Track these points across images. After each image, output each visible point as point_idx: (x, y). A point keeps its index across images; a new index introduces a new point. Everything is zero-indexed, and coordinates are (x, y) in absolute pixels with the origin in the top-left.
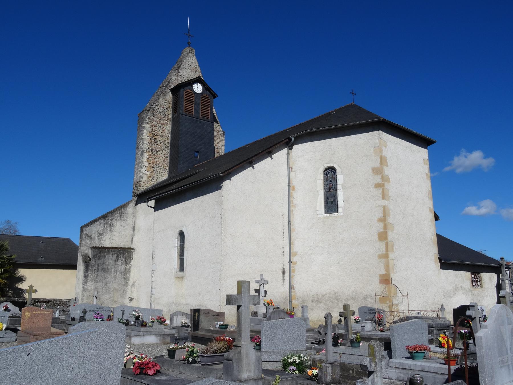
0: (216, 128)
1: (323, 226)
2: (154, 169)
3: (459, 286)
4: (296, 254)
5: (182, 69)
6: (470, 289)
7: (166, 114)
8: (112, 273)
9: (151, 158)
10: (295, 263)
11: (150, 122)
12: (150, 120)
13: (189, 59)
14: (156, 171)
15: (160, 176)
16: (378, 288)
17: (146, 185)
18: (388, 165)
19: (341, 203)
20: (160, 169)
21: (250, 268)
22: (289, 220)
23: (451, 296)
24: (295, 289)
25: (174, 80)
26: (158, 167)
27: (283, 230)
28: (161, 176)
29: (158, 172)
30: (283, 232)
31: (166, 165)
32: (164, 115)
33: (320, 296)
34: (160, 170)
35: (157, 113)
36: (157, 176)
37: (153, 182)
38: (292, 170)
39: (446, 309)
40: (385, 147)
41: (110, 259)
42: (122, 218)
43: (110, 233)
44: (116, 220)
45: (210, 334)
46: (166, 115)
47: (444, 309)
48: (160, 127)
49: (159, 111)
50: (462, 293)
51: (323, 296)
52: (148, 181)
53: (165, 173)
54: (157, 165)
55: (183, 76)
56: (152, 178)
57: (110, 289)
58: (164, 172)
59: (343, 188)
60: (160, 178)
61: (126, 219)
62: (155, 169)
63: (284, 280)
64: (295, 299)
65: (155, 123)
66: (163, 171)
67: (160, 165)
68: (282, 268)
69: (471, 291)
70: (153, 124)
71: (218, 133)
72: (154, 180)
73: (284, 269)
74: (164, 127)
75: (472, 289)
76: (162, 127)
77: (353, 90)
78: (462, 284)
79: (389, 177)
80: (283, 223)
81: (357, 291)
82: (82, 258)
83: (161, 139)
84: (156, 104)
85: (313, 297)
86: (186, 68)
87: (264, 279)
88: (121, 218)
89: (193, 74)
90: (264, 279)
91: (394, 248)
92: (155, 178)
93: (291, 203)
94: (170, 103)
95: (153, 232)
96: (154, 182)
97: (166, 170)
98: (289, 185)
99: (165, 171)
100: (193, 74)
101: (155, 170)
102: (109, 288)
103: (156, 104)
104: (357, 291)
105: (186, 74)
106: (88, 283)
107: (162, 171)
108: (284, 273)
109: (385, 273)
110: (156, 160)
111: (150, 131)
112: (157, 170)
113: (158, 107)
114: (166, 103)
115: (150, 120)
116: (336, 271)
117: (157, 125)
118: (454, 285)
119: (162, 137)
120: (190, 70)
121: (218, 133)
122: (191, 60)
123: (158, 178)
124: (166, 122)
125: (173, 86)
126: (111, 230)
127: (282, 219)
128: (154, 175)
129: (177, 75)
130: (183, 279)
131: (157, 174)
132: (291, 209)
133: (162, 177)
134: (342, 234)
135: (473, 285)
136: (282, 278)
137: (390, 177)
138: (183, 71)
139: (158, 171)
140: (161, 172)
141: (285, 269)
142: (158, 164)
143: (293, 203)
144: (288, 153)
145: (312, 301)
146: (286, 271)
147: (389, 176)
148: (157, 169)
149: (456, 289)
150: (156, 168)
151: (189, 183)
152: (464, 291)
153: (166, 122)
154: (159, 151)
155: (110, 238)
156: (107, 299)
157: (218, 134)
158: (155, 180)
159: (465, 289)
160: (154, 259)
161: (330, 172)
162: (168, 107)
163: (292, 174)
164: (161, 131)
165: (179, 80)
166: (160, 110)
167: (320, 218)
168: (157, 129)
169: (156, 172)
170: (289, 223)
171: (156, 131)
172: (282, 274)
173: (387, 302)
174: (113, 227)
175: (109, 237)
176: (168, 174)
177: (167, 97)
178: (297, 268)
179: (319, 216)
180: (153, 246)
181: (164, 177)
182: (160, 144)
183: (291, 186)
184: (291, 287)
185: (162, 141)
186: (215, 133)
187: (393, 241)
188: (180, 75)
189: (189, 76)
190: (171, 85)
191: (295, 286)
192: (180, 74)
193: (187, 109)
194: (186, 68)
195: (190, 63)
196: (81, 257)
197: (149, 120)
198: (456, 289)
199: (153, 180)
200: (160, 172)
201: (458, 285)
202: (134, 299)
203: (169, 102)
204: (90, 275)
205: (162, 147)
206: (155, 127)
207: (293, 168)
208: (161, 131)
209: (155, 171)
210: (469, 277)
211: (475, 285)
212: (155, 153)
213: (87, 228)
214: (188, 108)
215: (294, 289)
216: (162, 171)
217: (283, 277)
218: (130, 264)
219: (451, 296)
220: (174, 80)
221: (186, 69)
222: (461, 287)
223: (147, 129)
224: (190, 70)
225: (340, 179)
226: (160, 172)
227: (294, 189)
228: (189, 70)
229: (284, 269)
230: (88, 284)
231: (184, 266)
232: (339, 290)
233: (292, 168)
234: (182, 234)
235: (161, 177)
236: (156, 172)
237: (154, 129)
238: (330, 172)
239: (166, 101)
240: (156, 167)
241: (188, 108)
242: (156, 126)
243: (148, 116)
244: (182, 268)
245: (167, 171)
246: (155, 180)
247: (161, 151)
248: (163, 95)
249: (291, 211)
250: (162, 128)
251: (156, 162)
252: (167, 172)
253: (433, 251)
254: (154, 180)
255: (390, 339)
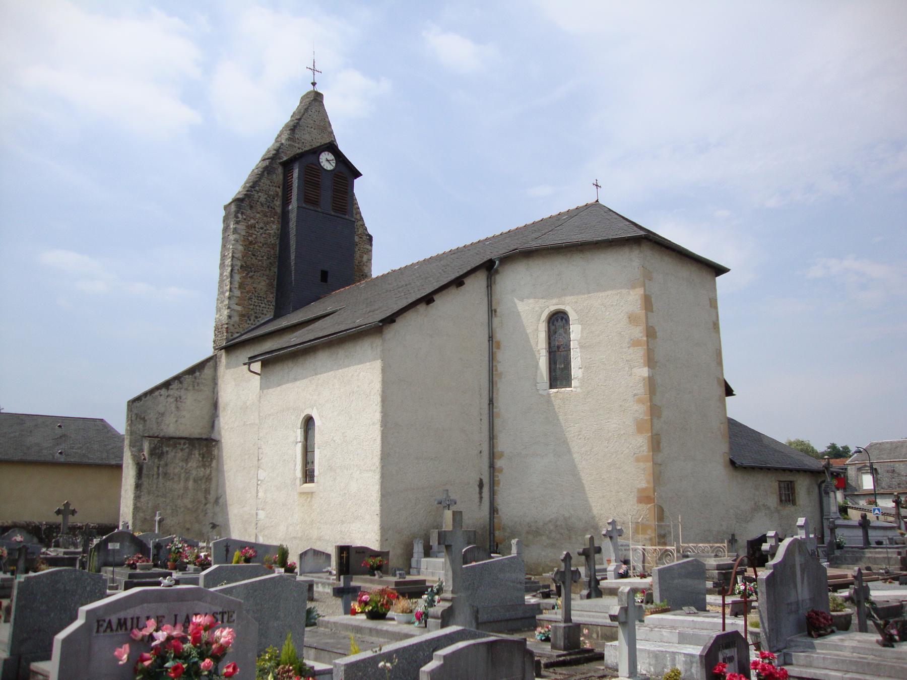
0: (358, 229)
1: (547, 410)
2: (250, 302)
3: (761, 503)
4: (502, 455)
5: (301, 128)
6: (776, 508)
7: (272, 205)
8: (182, 481)
9: (246, 283)
10: (501, 470)
11: (245, 219)
12: (245, 217)
13: (313, 111)
14: (254, 305)
15: (260, 315)
16: (634, 511)
17: (237, 330)
18: (654, 310)
19: (576, 370)
20: (260, 302)
21: (427, 479)
22: (490, 399)
23: (749, 519)
24: (500, 513)
25: (287, 148)
26: (257, 298)
27: (481, 415)
28: (263, 314)
29: (258, 308)
30: (481, 420)
31: (271, 296)
32: (268, 207)
33: (541, 524)
34: (260, 304)
35: (256, 203)
36: (256, 315)
37: (249, 324)
38: (495, 315)
39: (740, 541)
40: (650, 280)
41: (175, 457)
42: (196, 388)
43: (176, 412)
44: (186, 389)
45: (801, 606)
46: (271, 207)
47: (736, 541)
48: (262, 228)
49: (260, 201)
50: (764, 514)
51: (545, 524)
52: (241, 322)
53: (268, 308)
54: (256, 295)
55: (303, 141)
56: (246, 318)
57: (178, 509)
58: (267, 306)
59: (582, 347)
60: (260, 317)
61: (202, 388)
62: (251, 301)
63: (481, 498)
64: (499, 529)
65: (252, 221)
66: (266, 305)
67: (260, 295)
68: (479, 479)
69: (778, 511)
70: (250, 223)
71: (360, 238)
72: (250, 320)
73: (481, 480)
74: (268, 228)
75: (780, 508)
76: (265, 228)
77: (597, 180)
78: (764, 501)
79: (654, 329)
80: (480, 403)
81: (600, 516)
82: (131, 455)
83: (264, 249)
84: (255, 189)
85: (529, 525)
86: (307, 127)
87: (450, 497)
88: (194, 387)
89: (319, 137)
90: (450, 497)
91: (661, 445)
92: (252, 318)
93: (494, 368)
94: (279, 187)
95: (259, 415)
96: (250, 325)
97: (271, 303)
98: (491, 338)
99: (270, 305)
100: (319, 137)
101: (253, 303)
102: (176, 506)
103: (255, 189)
104: (600, 516)
105: (307, 137)
106: (142, 497)
107: (264, 305)
108: (481, 485)
109: (646, 485)
110: (255, 285)
111: (244, 236)
112: (256, 304)
113: (260, 194)
114: (273, 186)
115: (245, 217)
116: (567, 484)
117: (257, 224)
118: (753, 503)
119: (265, 246)
120: (314, 129)
121: (360, 238)
122: (317, 113)
123: (256, 317)
124: (272, 219)
125: (285, 159)
126: (178, 407)
127: (479, 396)
128: (250, 313)
129: (293, 139)
130: (314, 495)
131: (255, 311)
132: (495, 379)
133: (264, 316)
134: (579, 423)
135: (781, 501)
136: (477, 496)
137: (657, 330)
138: (303, 132)
139: (257, 306)
140: (263, 307)
141: (483, 480)
142: (257, 293)
143: (496, 370)
144: (489, 285)
145: (528, 533)
146: (484, 483)
147: (656, 328)
148: (255, 302)
149: (756, 509)
150: (254, 300)
151: (321, 335)
152: (767, 512)
153: (272, 219)
154: (259, 270)
155: (176, 421)
156: (173, 526)
157: (361, 239)
158: (252, 321)
159: (769, 508)
160: (260, 462)
161: (560, 320)
162: (276, 193)
163: (496, 321)
164: (264, 236)
165: (295, 147)
166: (262, 199)
167: (542, 395)
168: (256, 233)
169: (255, 307)
170: (491, 402)
171: (254, 236)
172: (477, 489)
173: (648, 532)
174: (181, 402)
175: (175, 420)
176: (273, 311)
177: (275, 176)
178: (501, 477)
179: (541, 392)
180: (259, 438)
181: (268, 316)
182: (261, 258)
183: (494, 340)
184: (493, 510)
185: (265, 253)
186: (357, 239)
187: (659, 435)
188: (298, 139)
189: (313, 140)
190: (282, 155)
191: (499, 507)
192: (297, 136)
193: (310, 198)
194: (307, 127)
195: (315, 117)
196: (130, 454)
197: (242, 216)
198: (756, 509)
199: (248, 322)
200: (260, 306)
201: (759, 502)
202: (218, 526)
203: (277, 185)
204: (145, 483)
205: (265, 263)
206: (253, 228)
207: (498, 310)
208: (264, 236)
209: (251, 304)
210: (711, 637)
211: (786, 500)
212: (253, 274)
213: (139, 404)
214: (311, 195)
215: (497, 514)
216: (264, 305)
217: (481, 493)
218: (211, 468)
219: (749, 519)
220: (287, 146)
221: (308, 129)
222: (764, 505)
223: (239, 232)
224: (314, 129)
225: (575, 331)
226: (260, 306)
227: (498, 348)
228: (312, 129)
229: (481, 480)
230: (142, 500)
231: (315, 475)
232: (571, 514)
233: (495, 311)
234: (309, 422)
235: (263, 316)
236: (255, 307)
237: (251, 232)
238: (560, 320)
239: (273, 184)
240: (254, 298)
241: (311, 195)
242: (255, 227)
243: (241, 210)
244: (308, 475)
245: (273, 305)
246: (252, 321)
247: (262, 270)
248: (268, 174)
249: (494, 383)
250: (266, 230)
251: (253, 289)
252: (272, 307)
253: (722, 448)
254: (250, 320)
255: (338, 546)
